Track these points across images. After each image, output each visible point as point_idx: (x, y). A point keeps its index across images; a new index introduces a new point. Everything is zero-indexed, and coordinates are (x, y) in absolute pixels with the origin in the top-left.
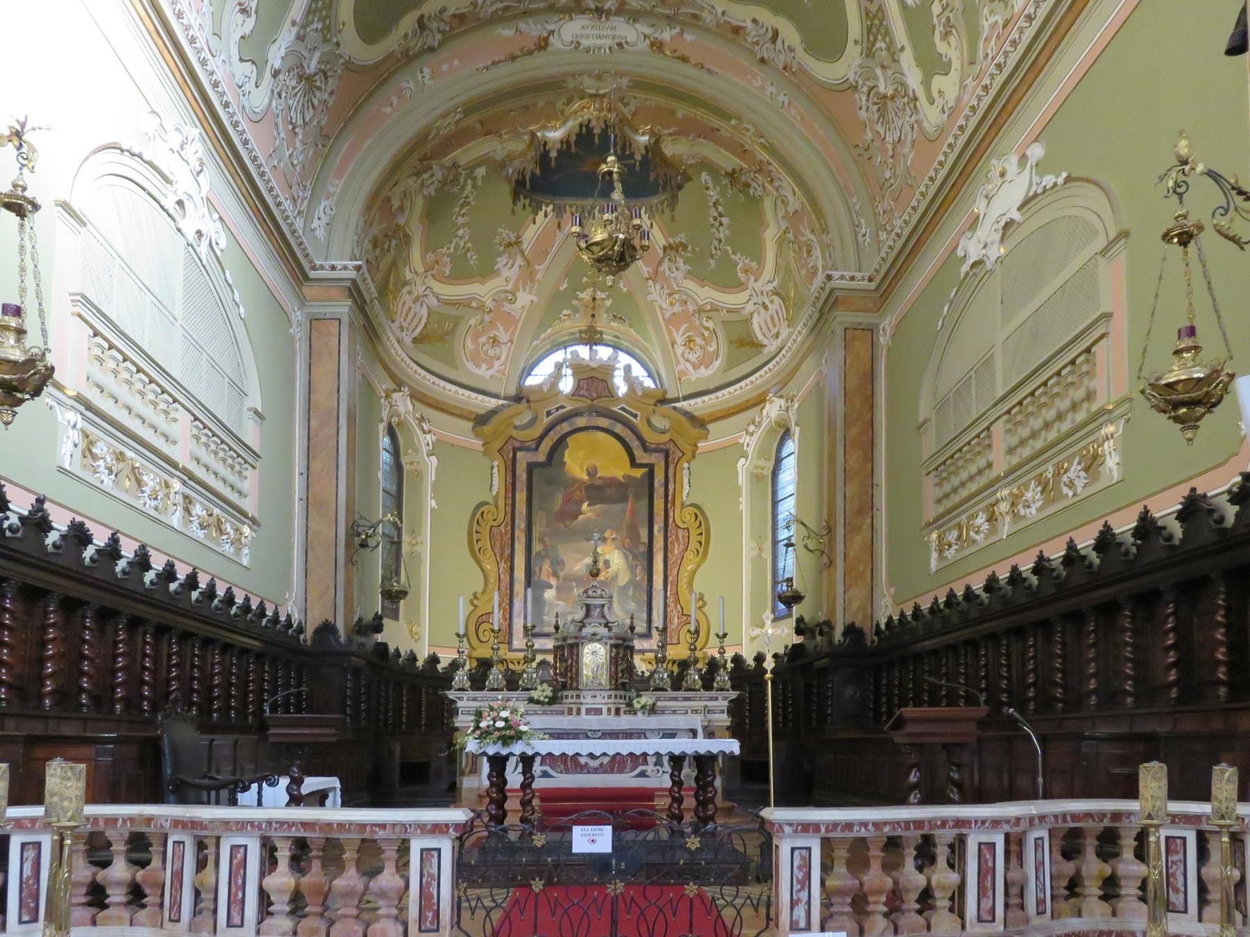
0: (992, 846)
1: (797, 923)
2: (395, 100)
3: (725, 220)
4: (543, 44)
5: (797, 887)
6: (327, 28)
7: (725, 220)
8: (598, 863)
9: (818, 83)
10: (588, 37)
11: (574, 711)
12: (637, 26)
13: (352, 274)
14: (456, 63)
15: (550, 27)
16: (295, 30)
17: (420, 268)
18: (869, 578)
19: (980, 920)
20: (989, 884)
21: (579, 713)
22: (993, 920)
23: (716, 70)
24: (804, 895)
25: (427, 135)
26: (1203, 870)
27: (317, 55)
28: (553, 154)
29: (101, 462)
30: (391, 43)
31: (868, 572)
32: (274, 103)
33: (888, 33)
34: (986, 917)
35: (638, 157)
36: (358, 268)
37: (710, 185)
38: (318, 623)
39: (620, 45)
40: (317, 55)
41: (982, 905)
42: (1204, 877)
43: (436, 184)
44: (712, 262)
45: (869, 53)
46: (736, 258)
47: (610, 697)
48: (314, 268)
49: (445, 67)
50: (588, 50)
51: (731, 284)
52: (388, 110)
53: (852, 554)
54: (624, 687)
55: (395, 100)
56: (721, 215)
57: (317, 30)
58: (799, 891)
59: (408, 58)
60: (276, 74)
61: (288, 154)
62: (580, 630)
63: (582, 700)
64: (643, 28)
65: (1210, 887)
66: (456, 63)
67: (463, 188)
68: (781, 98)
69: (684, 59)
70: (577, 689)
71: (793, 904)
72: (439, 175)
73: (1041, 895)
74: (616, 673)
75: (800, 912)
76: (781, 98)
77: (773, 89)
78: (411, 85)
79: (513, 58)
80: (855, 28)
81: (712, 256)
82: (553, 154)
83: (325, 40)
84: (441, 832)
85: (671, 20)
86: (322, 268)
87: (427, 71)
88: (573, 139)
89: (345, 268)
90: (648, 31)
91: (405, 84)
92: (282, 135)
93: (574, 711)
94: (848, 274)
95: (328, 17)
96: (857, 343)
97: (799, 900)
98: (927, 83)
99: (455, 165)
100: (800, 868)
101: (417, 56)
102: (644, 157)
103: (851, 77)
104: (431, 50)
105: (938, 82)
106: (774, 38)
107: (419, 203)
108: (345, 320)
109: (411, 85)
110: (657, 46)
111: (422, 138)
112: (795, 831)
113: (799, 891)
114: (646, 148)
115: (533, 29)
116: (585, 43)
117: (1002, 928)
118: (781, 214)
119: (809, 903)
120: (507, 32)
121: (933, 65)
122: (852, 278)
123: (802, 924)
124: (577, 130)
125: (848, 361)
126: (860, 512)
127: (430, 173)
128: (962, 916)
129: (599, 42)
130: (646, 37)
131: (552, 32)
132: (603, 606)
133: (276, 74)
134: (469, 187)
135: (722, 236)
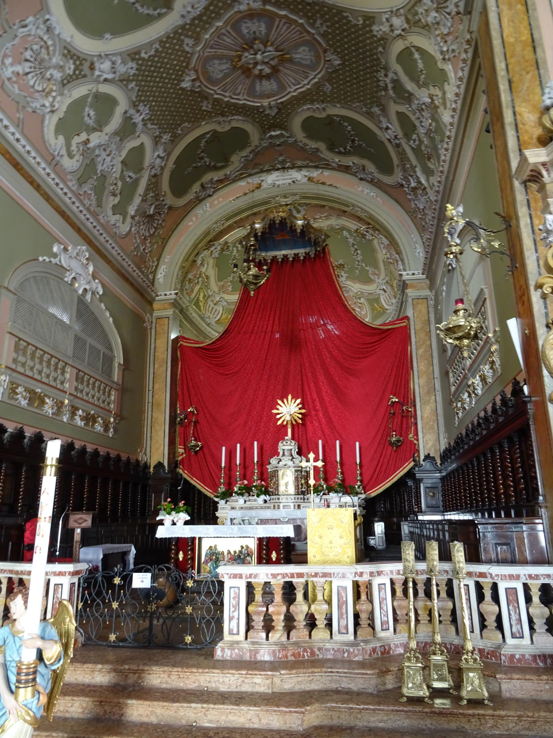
0: (345, 589)
1: (232, 630)
2: (194, 219)
3: (359, 252)
4: (259, 187)
5: (232, 609)
6: (157, 195)
7: (359, 252)
8: (146, 593)
9: (387, 185)
10: (279, 180)
11: (276, 507)
12: (302, 172)
13: (174, 296)
14: (221, 200)
15: (262, 179)
16: (140, 198)
17: (216, 289)
18: (436, 428)
19: (340, 632)
20: (344, 611)
21: (279, 508)
22: (347, 633)
23: (338, 186)
24: (236, 614)
25: (209, 232)
26: (480, 606)
27: (153, 207)
28: (259, 234)
29: (19, 396)
30: (190, 196)
31: (436, 425)
32: (133, 229)
33: (409, 161)
34: (344, 631)
35: (299, 231)
36: (176, 294)
37: (349, 236)
38: (156, 463)
39: (293, 182)
40: (153, 207)
41: (341, 624)
42: (250, 612)
43: (218, 252)
44: (357, 271)
45: (405, 170)
46: (367, 268)
47: (295, 499)
48: (157, 296)
49: (216, 202)
50: (279, 186)
51: (368, 281)
52: (191, 223)
53: (425, 416)
54: (303, 493)
55: (194, 219)
56: (356, 250)
57: (151, 197)
58: (233, 612)
59: (199, 200)
60: (133, 217)
61: (142, 248)
62: (278, 463)
63: (281, 501)
64: (304, 172)
65: (254, 617)
66: (221, 200)
67: (232, 252)
68: (372, 194)
69: (323, 183)
70: (278, 495)
71: (231, 619)
72: (219, 248)
73: (386, 619)
74: (298, 486)
75: (234, 623)
76: (372, 194)
77: (368, 191)
78: (201, 212)
79: (245, 194)
80: (396, 161)
81: (357, 268)
82: (259, 234)
83: (157, 200)
84: (62, 575)
85: (316, 167)
86: (161, 295)
87: (208, 205)
88: (267, 226)
89: (171, 294)
90: (307, 174)
91: (198, 212)
92: (139, 241)
93: (276, 507)
94: (410, 272)
95: (157, 190)
96: (420, 306)
97: (233, 617)
98: (428, 180)
99: (226, 243)
100: (234, 598)
101: (204, 199)
102: (302, 230)
103: (400, 181)
104: (210, 196)
105: (432, 179)
106: (364, 169)
107: (211, 261)
108: (171, 317)
109: (201, 212)
110: (310, 179)
111: (207, 233)
112: (230, 578)
113: (233, 612)
114: (303, 226)
115: (255, 180)
116: (277, 183)
117: (352, 638)
118: (382, 246)
119: (238, 619)
120: (242, 183)
121: (428, 172)
122: (413, 274)
123: (235, 631)
124: (269, 222)
125: (416, 315)
126: (428, 393)
127: (214, 247)
128: (374, 629)
129: (284, 182)
130: (306, 176)
131: (262, 181)
132: (291, 450)
133: (133, 217)
134: (235, 252)
135: (359, 259)
